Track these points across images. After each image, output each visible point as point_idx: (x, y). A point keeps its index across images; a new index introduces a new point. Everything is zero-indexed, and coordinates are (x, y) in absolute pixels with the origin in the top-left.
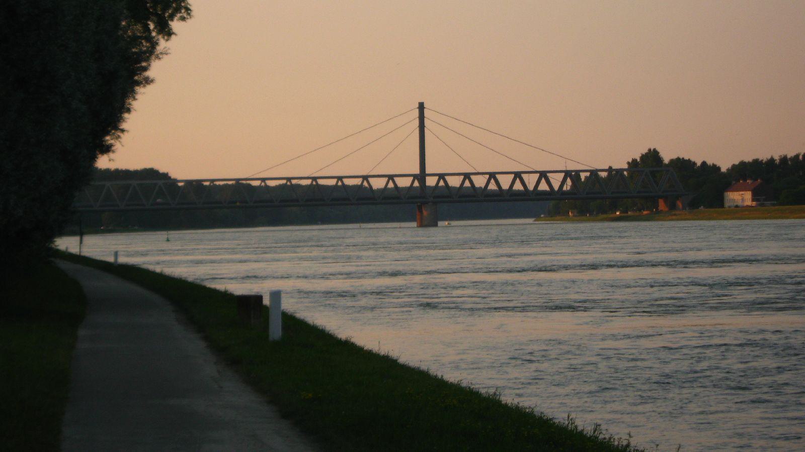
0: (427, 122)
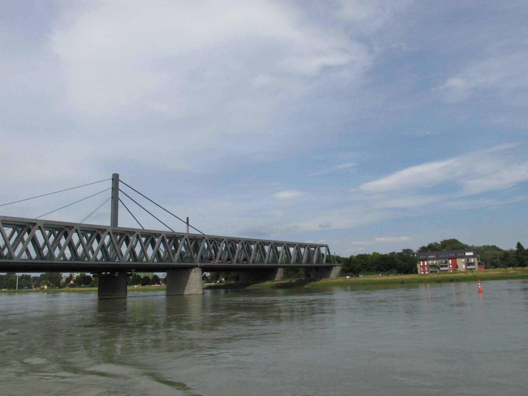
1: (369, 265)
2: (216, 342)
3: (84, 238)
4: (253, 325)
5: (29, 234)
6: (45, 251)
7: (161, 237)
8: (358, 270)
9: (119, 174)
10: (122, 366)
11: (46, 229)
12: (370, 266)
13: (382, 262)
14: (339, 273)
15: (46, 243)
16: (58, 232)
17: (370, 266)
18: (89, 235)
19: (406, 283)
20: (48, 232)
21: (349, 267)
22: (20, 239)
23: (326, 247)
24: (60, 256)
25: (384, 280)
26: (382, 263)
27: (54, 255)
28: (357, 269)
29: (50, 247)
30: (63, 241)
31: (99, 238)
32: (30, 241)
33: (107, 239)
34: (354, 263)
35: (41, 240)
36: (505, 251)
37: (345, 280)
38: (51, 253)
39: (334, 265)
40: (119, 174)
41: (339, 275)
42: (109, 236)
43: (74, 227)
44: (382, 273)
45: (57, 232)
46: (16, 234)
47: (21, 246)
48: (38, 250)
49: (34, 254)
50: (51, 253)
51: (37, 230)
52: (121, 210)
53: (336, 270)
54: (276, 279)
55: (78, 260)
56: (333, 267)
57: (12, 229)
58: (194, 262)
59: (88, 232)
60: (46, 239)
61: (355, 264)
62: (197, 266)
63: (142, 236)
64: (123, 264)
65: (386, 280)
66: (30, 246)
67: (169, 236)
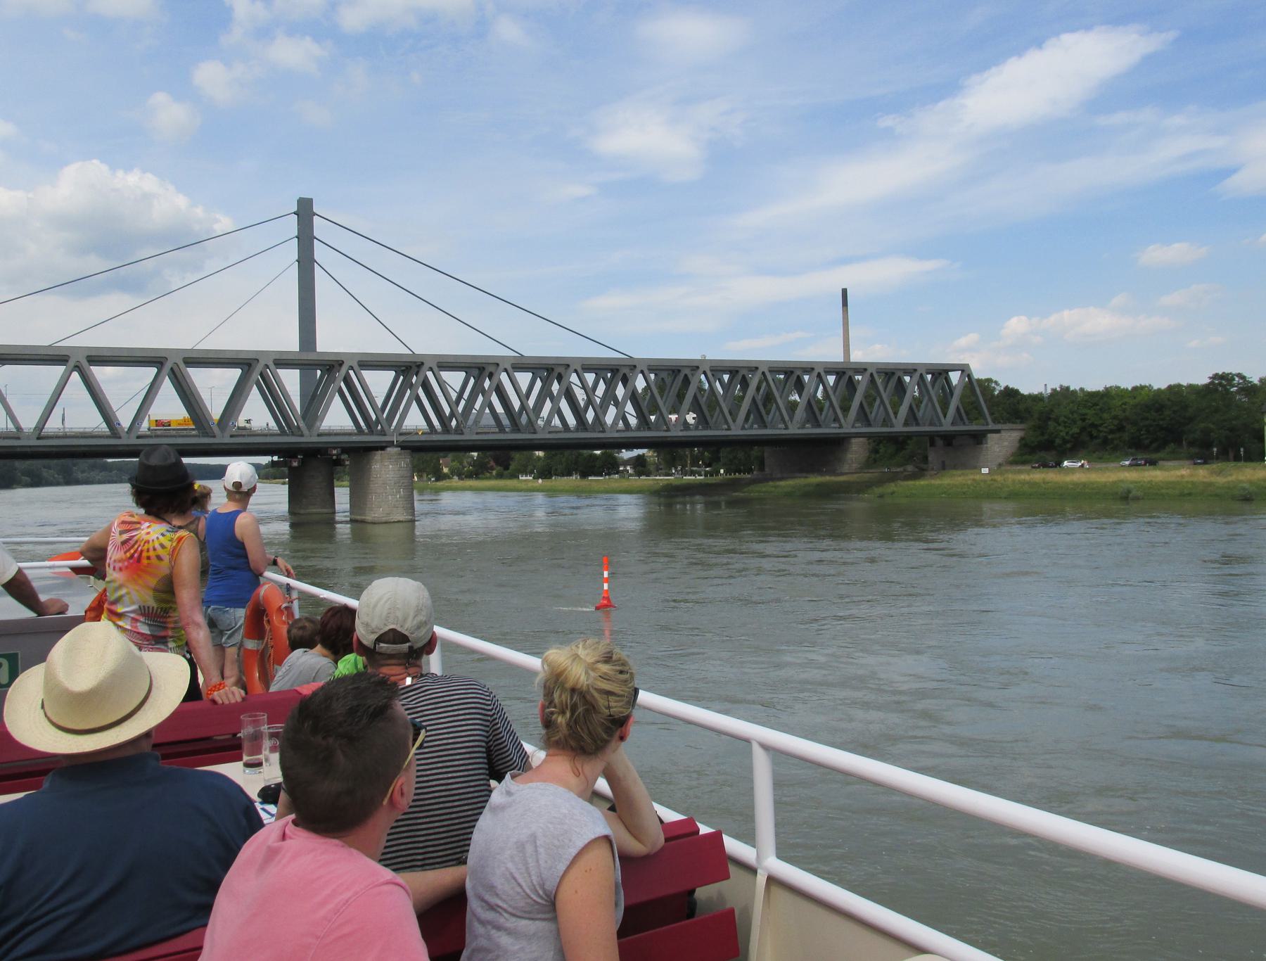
0: (319, 252)
1: (1106, 427)
2: (287, 678)
3: (718, 383)
4: (933, 541)
5: (559, 383)
6: (590, 415)
7: (815, 374)
8: (1069, 446)
9: (312, 199)
10: (1033, 526)
11: (515, 370)
12: (1112, 432)
13: (1147, 419)
14: (1013, 455)
15: (590, 402)
16: (728, 376)
17: (1112, 432)
18: (726, 377)
19: (1137, 499)
20: (909, 378)
21: (1043, 434)
22: (545, 393)
23: (963, 371)
24: (615, 422)
25: (1076, 485)
26: (1147, 423)
27: (606, 423)
28: (1065, 442)
29: (598, 410)
30: (620, 391)
31: (625, 381)
32: (414, 401)
33: (640, 384)
34: (1056, 420)
35: (580, 395)
36: (600, 811)
37: (977, 477)
38: (598, 419)
39: (991, 426)
40: (312, 199)
41: (1011, 458)
42: (505, 373)
43: (816, 368)
44: (1132, 454)
45: (609, 375)
46: (539, 384)
47: (548, 405)
48: (578, 413)
49: (571, 421)
50: (598, 419)
51: (503, 373)
52: (321, 282)
53: (1003, 442)
54: (846, 468)
55: (649, 429)
56: (989, 435)
57: (531, 374)
58: (892, 426)
59: (725, 372)
60: (590, 392)
61: (1059, 425)
62: (391, 444)
63: (829, 372)
64: (128, 445)
65: (1085, 485)
66: (564, 405)
67: (673, 368)
